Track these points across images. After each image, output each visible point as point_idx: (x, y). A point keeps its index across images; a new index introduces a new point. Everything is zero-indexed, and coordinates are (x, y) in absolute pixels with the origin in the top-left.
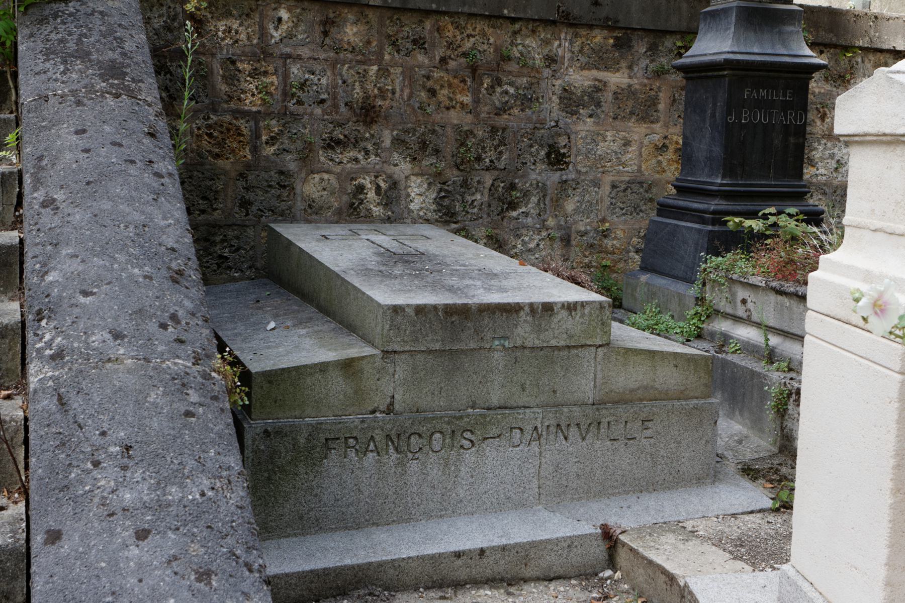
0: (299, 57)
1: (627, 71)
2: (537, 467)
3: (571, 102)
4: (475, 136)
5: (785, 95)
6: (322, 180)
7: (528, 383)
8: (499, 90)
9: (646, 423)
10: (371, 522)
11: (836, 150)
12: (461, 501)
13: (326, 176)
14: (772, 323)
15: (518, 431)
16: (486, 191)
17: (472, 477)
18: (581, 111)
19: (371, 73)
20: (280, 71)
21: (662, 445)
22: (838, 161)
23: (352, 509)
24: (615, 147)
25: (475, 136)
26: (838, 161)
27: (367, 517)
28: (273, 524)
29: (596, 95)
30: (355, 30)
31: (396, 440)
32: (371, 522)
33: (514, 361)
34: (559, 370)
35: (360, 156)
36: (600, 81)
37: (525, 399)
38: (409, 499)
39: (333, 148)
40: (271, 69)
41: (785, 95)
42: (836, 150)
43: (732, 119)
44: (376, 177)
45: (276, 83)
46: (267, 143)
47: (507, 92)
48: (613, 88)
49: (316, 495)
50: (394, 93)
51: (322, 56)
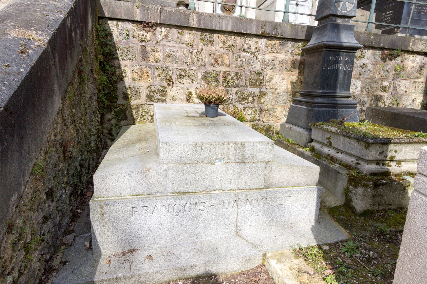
0: (169, 46)
1: (284, 53)
2: (236, 218)
3: (264, 64)
4: (231, 76)
5: (345, 59)
6: (177, 89)
7: (233, 179)
8: (239, 59)
9: (288, 198)
10: (156, 243)
11: (356, 83)
12: (200, 233)
13: (178, 88)
14: (341, 148)
15: (227, 202)
16: (234, 95)
17: (205, 223)
18: (268, 67)
19: (194, 52)
20: (162, 51)
21: (295, 207)
22: (356, 86)
23: (147, 238)
24: (279, 80)
25: (231, 76)
26: (356, 86)
27: (154, 242)
28: (107, 246)
29: (273, 62)
30: (189, 36)
31: (167, 207)
32: (156, 243)
33: (226, 169)
34: (248, 173)
35: (190, 82)
36: (275, 57)
37: (231, 186)
38: (175, 233)
39: (180, 78)
40: (159, 50)
41: (345, 59)
42: (356, 83)
43: (324, 68)
44: (196, 89)
45: (160, 55)
46: (157, 76)
47: (242, 60)
48: (280, 60)
49: (128, 233)
50: (202, 60)
51: (177, 46)
